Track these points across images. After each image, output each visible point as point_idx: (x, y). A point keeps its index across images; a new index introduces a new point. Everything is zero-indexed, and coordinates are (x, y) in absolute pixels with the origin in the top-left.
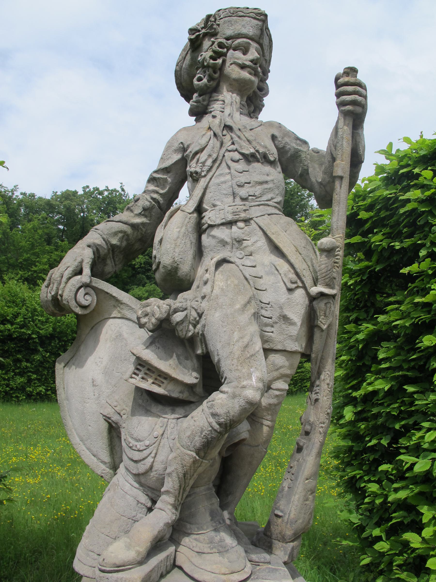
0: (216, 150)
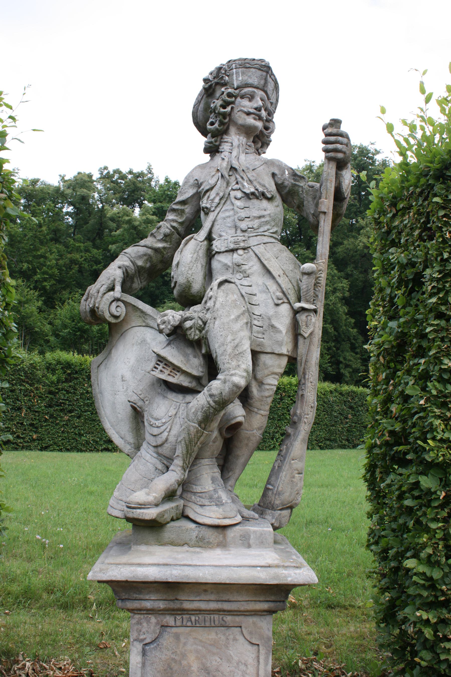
0: (222, 189)
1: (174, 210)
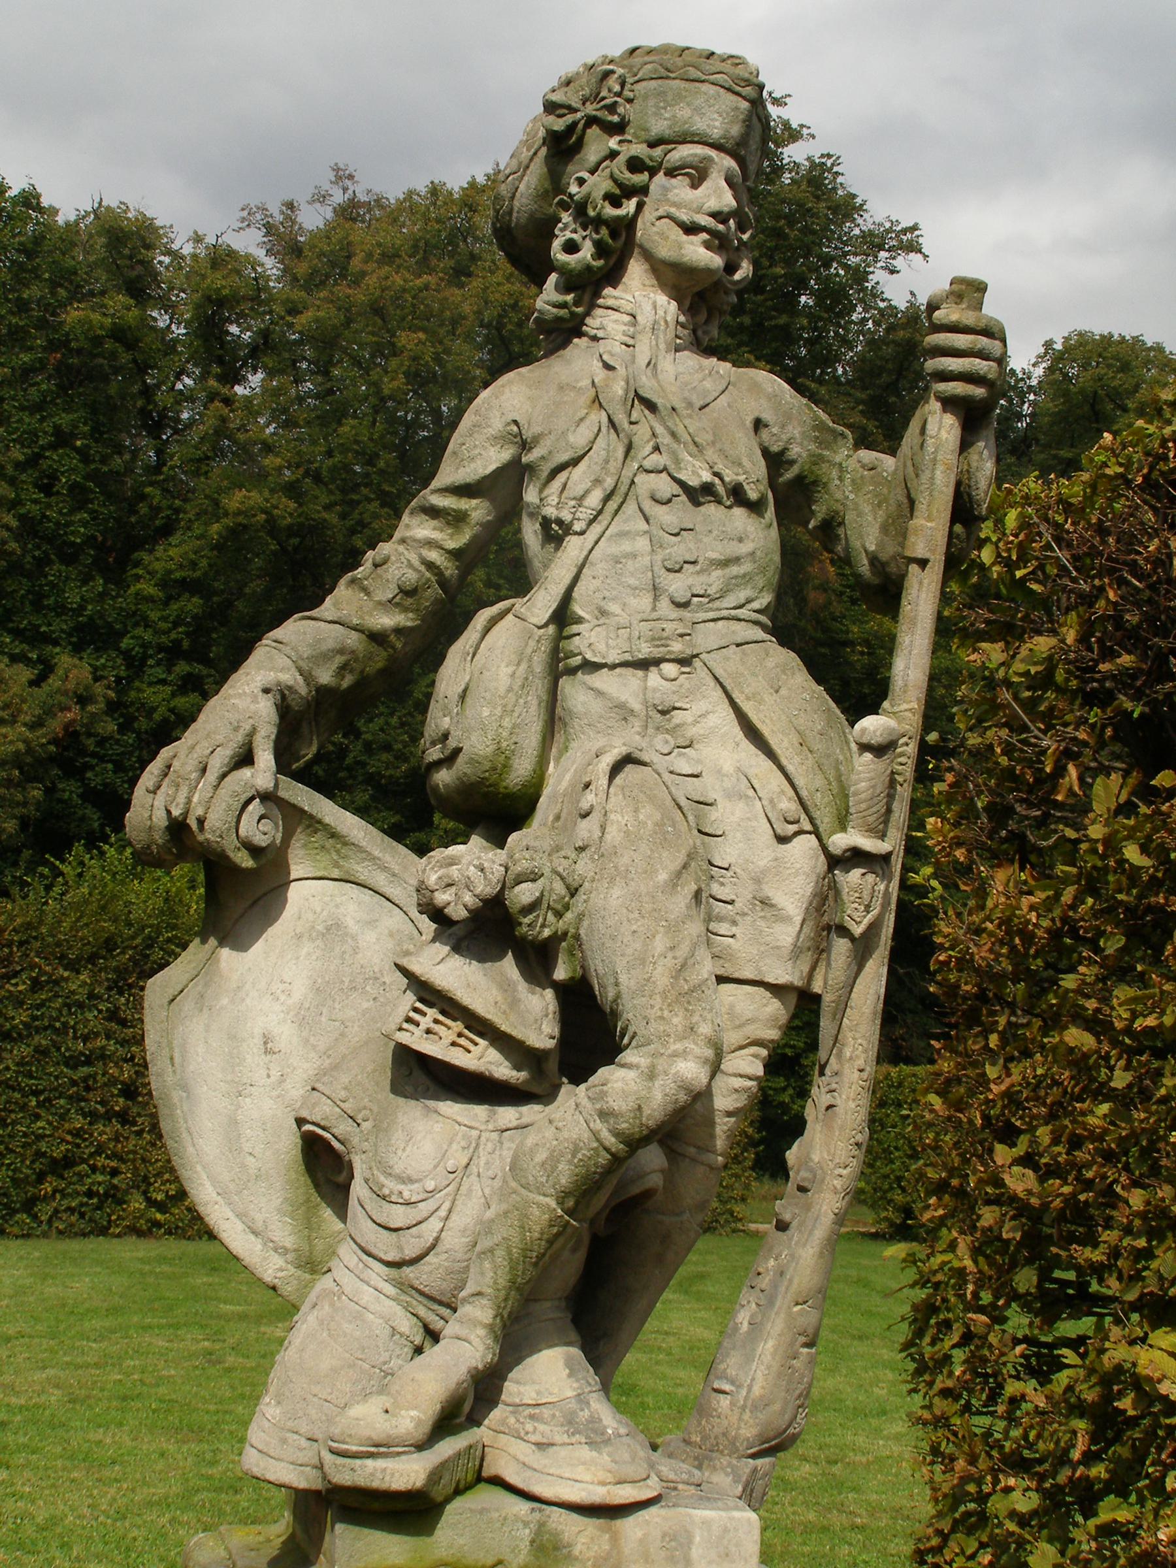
0: (614, 466)
1: (433, 512)
